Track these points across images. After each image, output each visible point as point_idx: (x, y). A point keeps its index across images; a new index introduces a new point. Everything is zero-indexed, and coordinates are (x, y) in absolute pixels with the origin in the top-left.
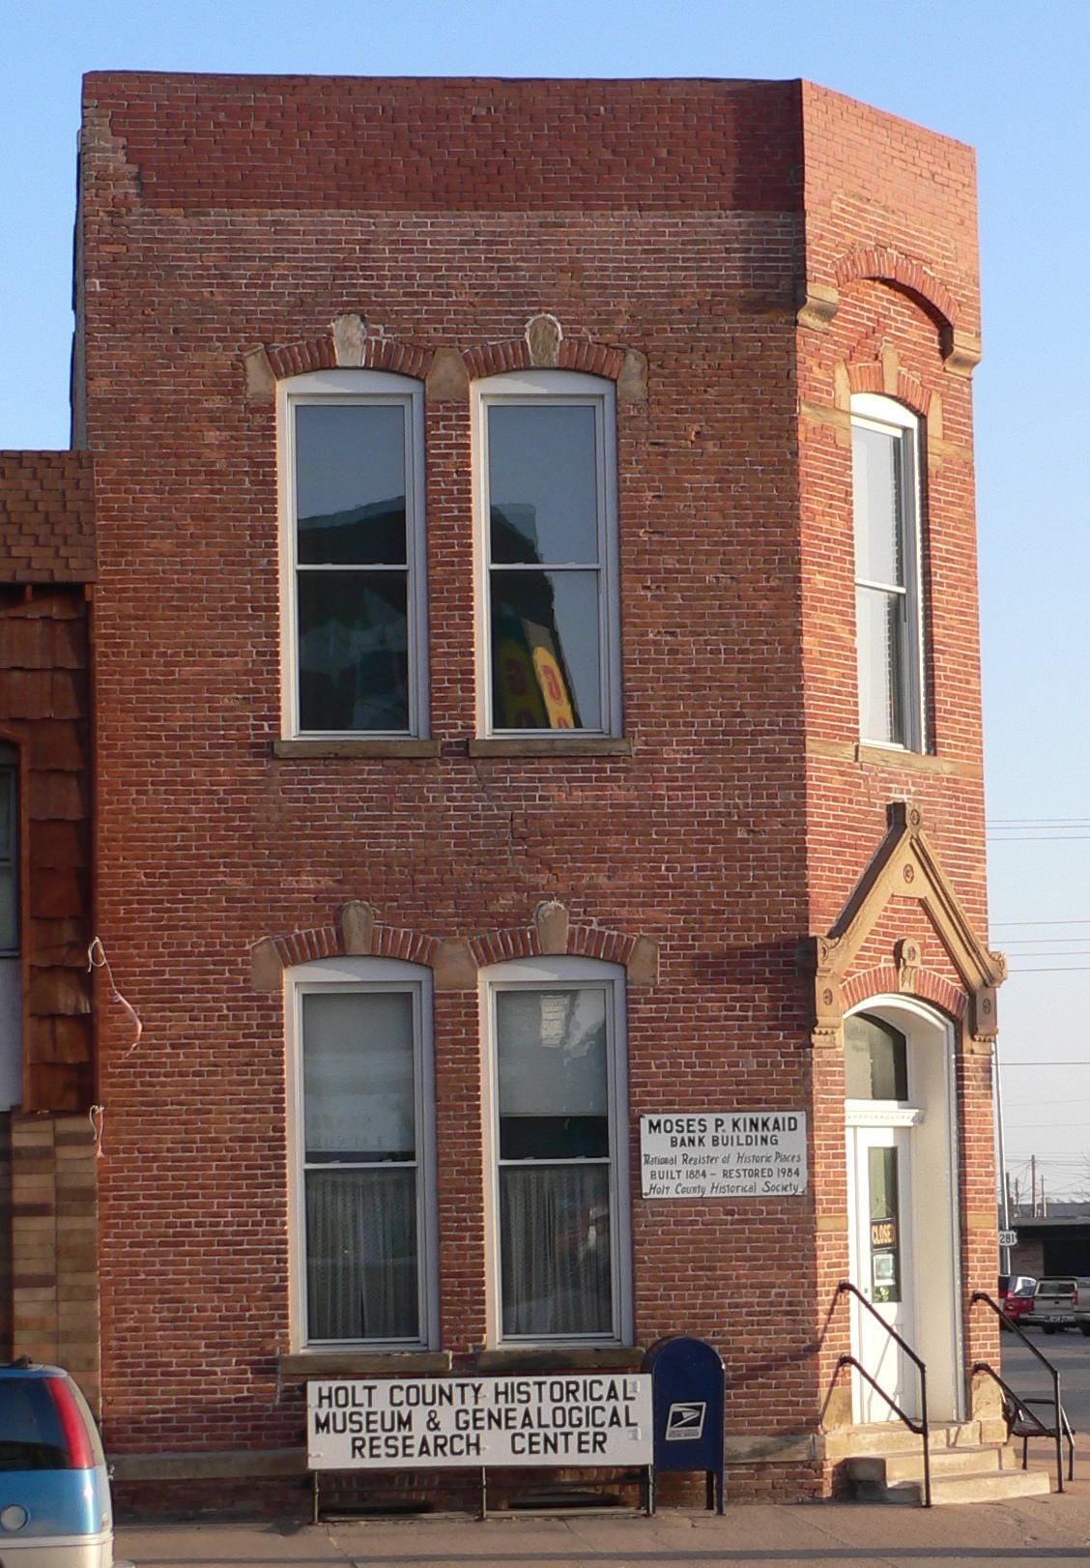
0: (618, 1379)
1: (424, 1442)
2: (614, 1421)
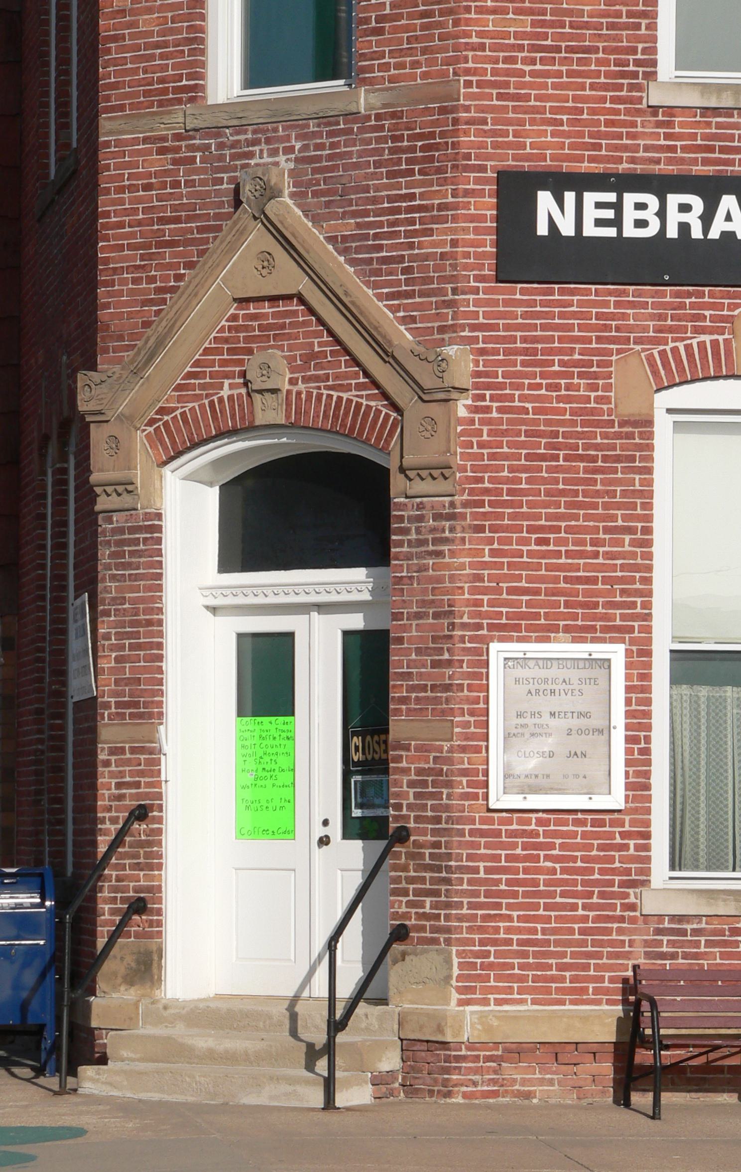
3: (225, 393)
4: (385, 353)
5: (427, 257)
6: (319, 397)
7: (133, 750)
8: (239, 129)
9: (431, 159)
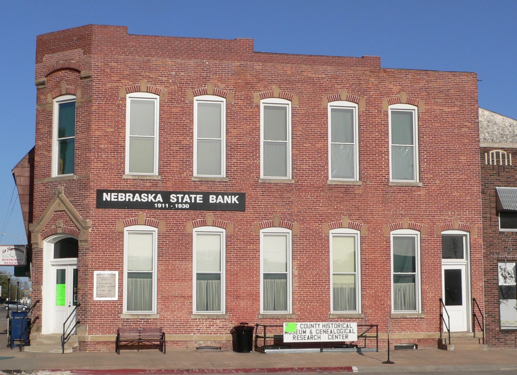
0: (349, 324)
1: (308, 337)
2: (350, 332)
3: (53, 227)
4: (78, 221)
8: (56, 182)
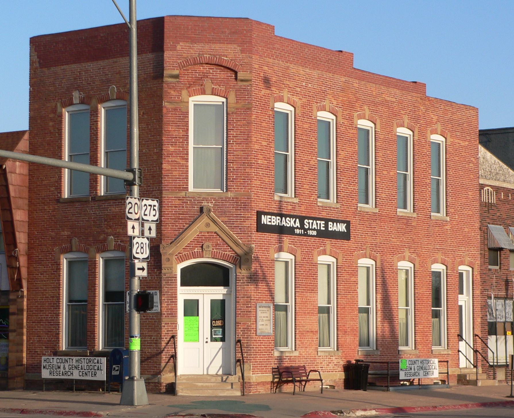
0: (99, 358)
2: (98, 369)
3: (196, 250)
5: (245, 226)
6: (219, 253)
7: (171, 324)
9: (245, 208)
